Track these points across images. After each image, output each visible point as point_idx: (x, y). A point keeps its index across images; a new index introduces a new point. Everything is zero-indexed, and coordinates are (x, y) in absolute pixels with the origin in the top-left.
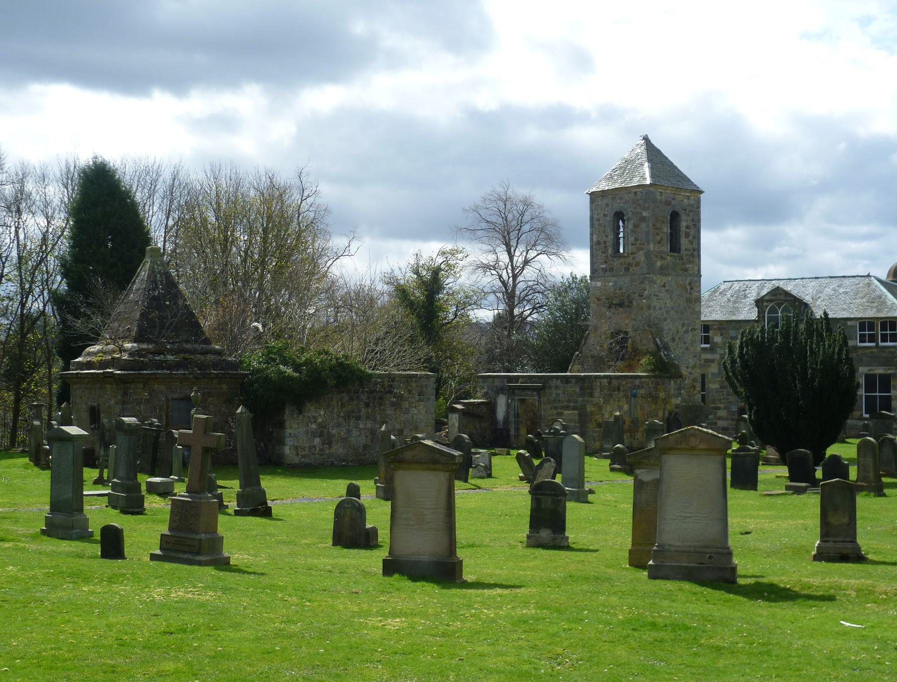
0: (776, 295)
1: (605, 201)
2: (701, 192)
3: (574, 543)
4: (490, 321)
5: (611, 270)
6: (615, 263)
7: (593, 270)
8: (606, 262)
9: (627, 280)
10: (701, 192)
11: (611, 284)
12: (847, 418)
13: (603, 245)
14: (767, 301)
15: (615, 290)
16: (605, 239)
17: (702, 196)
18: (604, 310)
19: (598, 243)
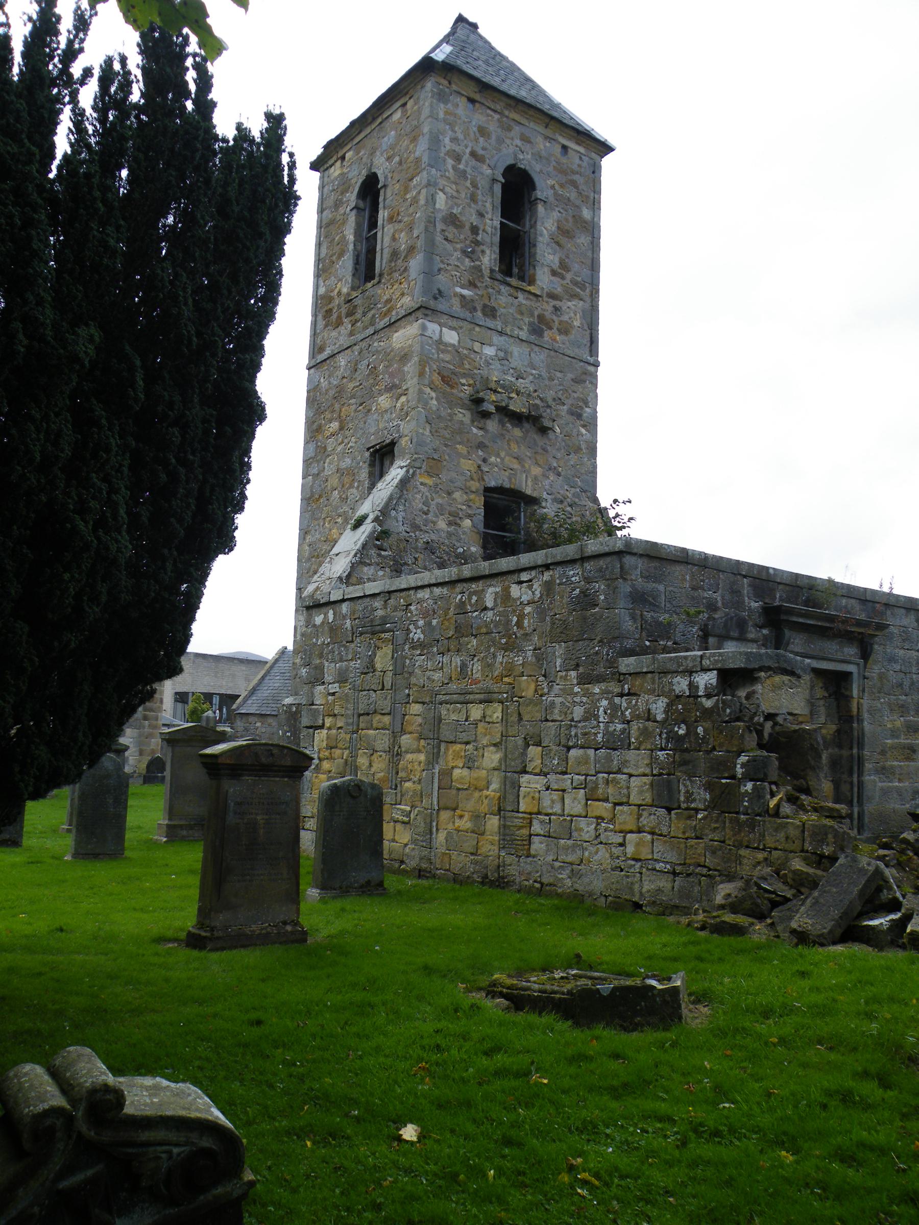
2: (606, 148)
5: (490, 312)
8: (472, 285)
10: (606, 148)
11: (489, 351)
16: (474, 219)
17: (607, 162)
18: (464, 416)
19: (452, 220)
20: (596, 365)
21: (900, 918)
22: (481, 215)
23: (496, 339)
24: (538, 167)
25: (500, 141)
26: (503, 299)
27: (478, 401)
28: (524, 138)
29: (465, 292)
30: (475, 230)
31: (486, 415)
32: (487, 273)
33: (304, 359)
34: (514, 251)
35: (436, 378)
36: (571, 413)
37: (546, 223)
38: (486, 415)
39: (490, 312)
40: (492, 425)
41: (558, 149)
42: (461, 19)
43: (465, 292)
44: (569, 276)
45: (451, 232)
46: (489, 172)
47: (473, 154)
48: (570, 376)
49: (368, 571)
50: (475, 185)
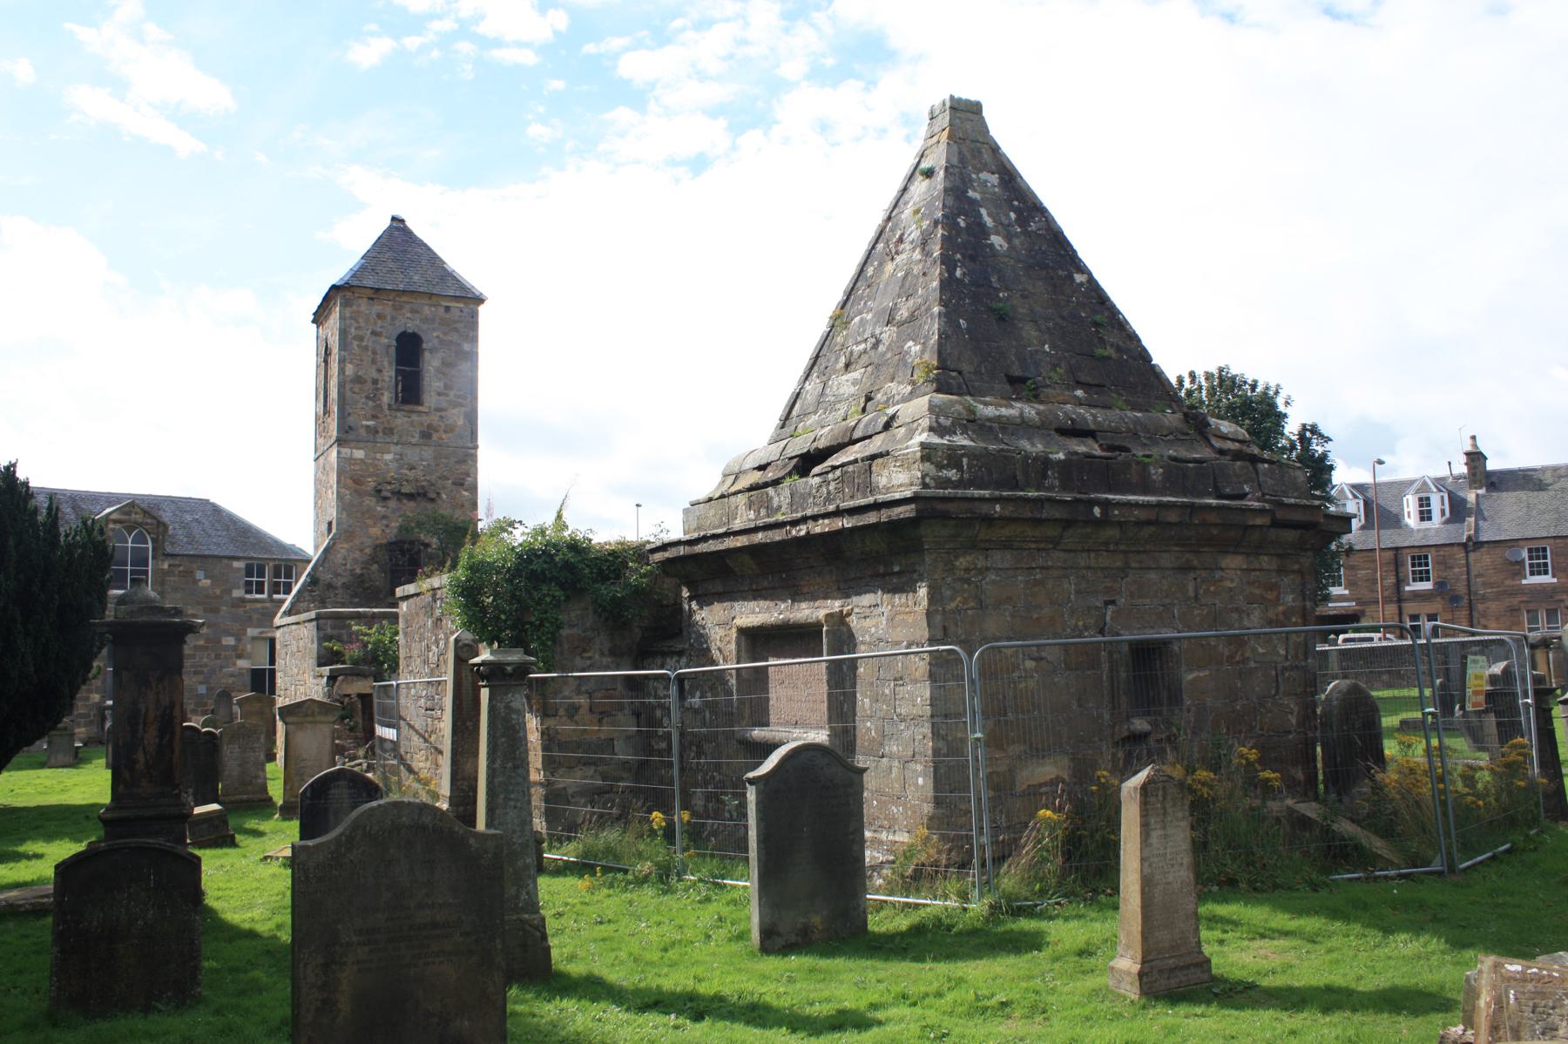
0: (128, 513)
1: (377, 308)
2: (480, 300)
3: (572, 958)
4: (18, 475)
5: (389, 431)
6: (399, 421)
7: (1493, 473)
8: (374, 417)
9: (428, 453)
10: (480, 300)
11: (388, 457)
12: (865, 891)
13: (369, 385)
14: (115, 522)
15: (401, 467)
16: (375, 375)
17: (481, 309)
18: (370, 502)
19: (358, 380)
20: (476, 447)
21: (34, 839)
22: (380, 371)
23: (393, 448)
24: (425, 327)
25: (394, 318)
26: (400, 420)
27: (379, 491)
28: (413, 311)
29: (370, 423)
30: (375, 382)
31: (385, 499)
32: (385, 407)
33: (312, 456)
34: (410, 390)
35: (349, 482)
36: (454, 483)
37: (431, 364)
38: (385, 499)
39: (389, 431)
40: (393, 504)
41: (442, 310)
42: (394, 219)
43: (370, 423)
44: (452, 394)
45: (357, 387)
46: (388, 341)
47: (374, 333)
48: (453, 459)
49: (303, 605)
50: (374, 353)
